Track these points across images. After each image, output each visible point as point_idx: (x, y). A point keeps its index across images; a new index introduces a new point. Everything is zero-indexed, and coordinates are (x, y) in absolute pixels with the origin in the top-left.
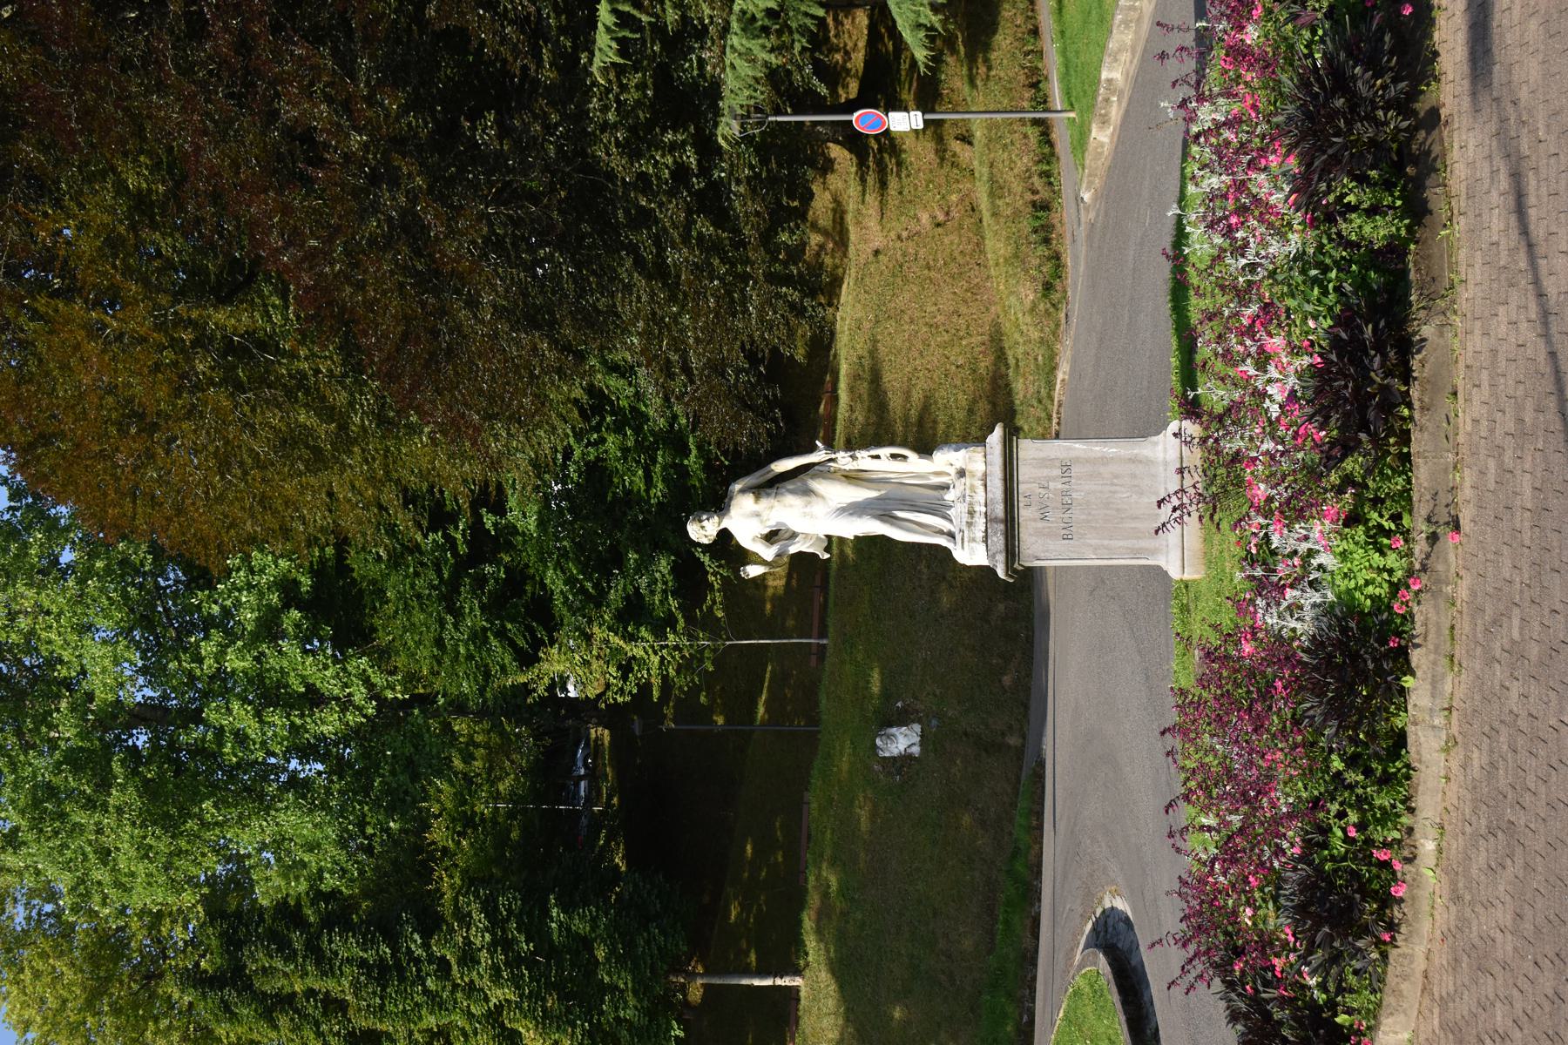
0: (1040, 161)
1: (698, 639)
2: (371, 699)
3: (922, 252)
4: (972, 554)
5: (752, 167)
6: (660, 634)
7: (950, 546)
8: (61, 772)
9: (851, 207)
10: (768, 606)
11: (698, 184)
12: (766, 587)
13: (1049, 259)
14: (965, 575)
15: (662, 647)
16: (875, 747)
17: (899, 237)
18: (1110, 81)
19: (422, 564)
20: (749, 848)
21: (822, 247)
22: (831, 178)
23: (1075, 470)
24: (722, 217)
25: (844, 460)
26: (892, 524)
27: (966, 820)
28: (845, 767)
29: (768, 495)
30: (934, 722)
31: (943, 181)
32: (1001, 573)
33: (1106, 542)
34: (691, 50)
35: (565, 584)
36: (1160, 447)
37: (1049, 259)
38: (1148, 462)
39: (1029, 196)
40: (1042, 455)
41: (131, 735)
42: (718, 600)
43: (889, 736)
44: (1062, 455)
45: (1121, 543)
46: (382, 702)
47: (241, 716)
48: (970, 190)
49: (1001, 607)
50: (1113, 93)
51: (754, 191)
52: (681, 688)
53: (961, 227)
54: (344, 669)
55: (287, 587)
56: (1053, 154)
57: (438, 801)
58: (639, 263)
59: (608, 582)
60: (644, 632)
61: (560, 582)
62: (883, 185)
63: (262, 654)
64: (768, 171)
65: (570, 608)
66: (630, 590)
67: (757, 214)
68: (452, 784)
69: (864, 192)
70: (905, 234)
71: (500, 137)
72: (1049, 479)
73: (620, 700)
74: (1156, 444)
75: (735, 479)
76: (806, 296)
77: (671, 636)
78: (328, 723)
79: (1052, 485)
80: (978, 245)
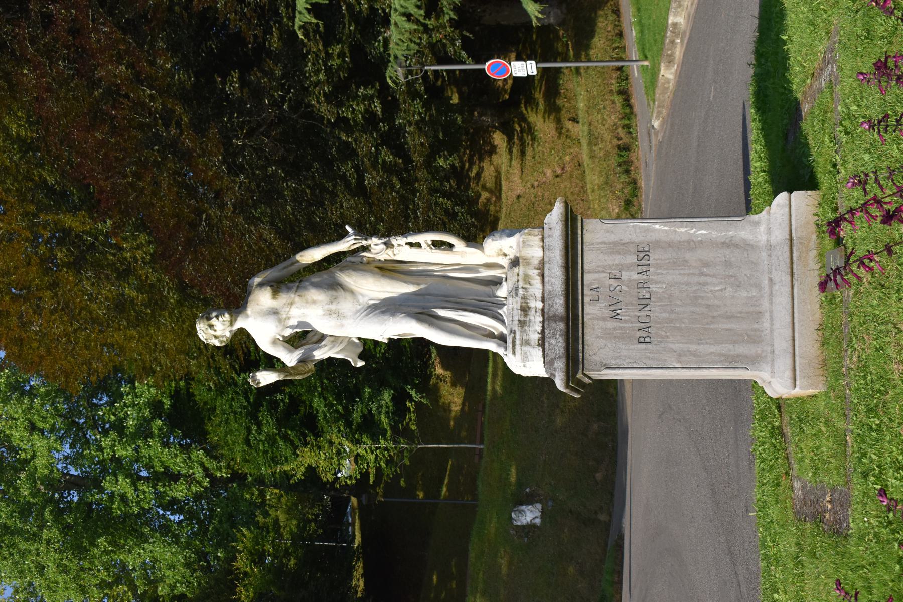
0: (623, 118)
1: (399, 443)
2: (206, 476)
4: (528, 364)
5: (420, 114)
6: (375, 441)
7: (500, 351)
8: (12, 517)
9: (504, 168)
10: (452, 423)
11: (383, 127)
12: (450, 411)
13: (629, 183)
14: (572, 404)
15: (377, 449)
16: (511, 518)
17: (533, 186)
18: (675, 25)
19: (237, 393)
20: (435, 577)
21: (488, 200)
22: (494, 157)
23: (654, 256)
24: (400, 150)
25: (377, 248)
26: (431, 324)
27: (571, 570)
28: (493, 531)
29: (289, 289)
30: (550, 503)
31: (560, 147)
32: (560, 384)
33: (693, 347)
34: (379, 33)
35: (325, 407)
36: (762, 228)
37: (629, 183)
38: (747, 247)
39: (615, 142)
40: (613, 238)
41: (69, 494)
42: (413, 418)
43: (520, 512)
44: (638, 238)
45: (712, 349)
46: (213, 480)
47: (123, 485)
50: (677, 36)
51: (420, 129)
52: (388, 475)
53: (571, 176)
54: (189, 458)
55: (156, 406)
56: (632, 113)
57: (243, 542)
58: (347, 185)
59: (353, 406)
60: (365, 439)
62: (523, 153)
63: (139, 446)
64: (431, 116)
65: (327, 422)
66: (366, 412)
67: (422, 145)
68: (251, 532)
69: (511, 159)
70: (536, 183)
71: (241, 87)
72: (622, 268)
73: (349, 482)
74: (757, 223)
75: (253, 274)
77: (382, 442)
78: (179, 491)
79: (625, 276)
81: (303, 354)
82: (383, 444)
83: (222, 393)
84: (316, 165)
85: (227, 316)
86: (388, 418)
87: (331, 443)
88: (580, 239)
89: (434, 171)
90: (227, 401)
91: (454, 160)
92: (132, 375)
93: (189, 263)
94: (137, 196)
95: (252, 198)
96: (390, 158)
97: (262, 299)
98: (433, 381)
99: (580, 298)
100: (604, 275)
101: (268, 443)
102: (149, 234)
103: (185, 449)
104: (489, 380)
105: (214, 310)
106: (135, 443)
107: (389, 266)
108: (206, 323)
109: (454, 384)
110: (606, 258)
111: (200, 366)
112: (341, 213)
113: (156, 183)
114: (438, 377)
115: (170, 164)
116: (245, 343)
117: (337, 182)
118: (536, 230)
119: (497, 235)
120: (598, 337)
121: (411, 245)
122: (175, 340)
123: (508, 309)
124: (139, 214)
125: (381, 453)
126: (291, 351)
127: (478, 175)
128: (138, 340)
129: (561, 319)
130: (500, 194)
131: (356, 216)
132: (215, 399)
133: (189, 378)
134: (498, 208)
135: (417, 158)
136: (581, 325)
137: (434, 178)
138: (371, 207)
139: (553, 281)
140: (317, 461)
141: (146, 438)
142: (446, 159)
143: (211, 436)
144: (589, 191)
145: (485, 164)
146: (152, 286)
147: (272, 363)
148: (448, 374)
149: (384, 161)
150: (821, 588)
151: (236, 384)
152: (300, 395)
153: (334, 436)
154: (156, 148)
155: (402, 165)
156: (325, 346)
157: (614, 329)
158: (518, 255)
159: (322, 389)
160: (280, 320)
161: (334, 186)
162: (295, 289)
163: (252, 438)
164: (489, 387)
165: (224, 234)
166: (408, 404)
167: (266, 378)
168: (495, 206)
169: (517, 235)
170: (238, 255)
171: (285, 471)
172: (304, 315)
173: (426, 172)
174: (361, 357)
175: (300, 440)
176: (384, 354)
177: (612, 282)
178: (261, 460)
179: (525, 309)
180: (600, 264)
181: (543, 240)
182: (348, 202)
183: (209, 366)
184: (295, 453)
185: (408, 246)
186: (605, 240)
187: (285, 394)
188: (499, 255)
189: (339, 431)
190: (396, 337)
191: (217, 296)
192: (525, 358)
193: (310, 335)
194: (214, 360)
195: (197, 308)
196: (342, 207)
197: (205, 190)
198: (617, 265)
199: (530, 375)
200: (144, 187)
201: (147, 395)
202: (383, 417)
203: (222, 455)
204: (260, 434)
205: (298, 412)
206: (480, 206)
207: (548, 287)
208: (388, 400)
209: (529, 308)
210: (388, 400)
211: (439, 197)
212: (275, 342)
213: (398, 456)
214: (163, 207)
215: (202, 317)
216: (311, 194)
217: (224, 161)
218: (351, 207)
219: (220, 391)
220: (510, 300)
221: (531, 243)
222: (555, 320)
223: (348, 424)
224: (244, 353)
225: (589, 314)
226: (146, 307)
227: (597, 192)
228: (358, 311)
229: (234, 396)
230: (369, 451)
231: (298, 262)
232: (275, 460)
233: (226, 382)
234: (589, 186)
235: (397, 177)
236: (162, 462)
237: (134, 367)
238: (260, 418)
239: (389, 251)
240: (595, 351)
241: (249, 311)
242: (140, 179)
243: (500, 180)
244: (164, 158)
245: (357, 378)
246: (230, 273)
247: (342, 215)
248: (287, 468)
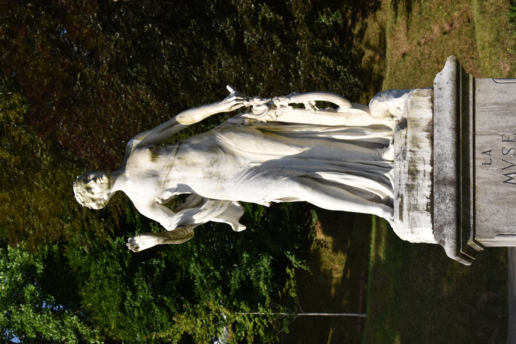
1: (279, 311)
3: (433, 52)
4: (416, 230)
6: (254, 308)
7: (387, 216)
9: (388, 25)
10: (333, 291)
12: (332, 278)
15: (255, 316)
17: (419, 44)
19: (111, 257)
21: (372, 58)
22: (379, 13)
25: (259, 110)
26: (315, 188)
29: (168, 151)
32: (449, 251)
35: (202, 273)
40: (506, 98)
42: (293, 285)
48: (468, 8)
49: (485, 296)
53: (460, 33)
54: (63, 324)
55: (28, 271)
58: (226, 43)
59: (231, 272)
60: (243, 306)
61: (199, 271)
62: (409, 9)
63: (11, 312)
65: (204, 288)
66: (244, 278)
69: (396, 16)
70: (423, 41)
75: (134, 135)
76: (340, 64)
77: (261, 309)
80: (472, 45)
81: (183, 218)
82: (261, 311)
83: (96, 258)
84: (193, 22)
85: (105, 179)
86: (267, 284)
87: (208, 310)
88: (471, 100)
89: (317, 30)
90: (102, 265)
91: (336, 17)
92: (4, 238)
93: (64, 123)
94: (10, 55)
95: (128, 57)
96: (270, 15)
97: (141, 161)
98: (313, 247)
99: (471, 161)
100: (497, 137)
101: (143, 309)
102: (22, 94)
103: (59, 315)
104: (372, 246)
105: (92, 173)
106: (6, 309)
107: (272, 127)
108: (84, 185)
109: (335, 250)
110: (499, 119)
111: (74, 230)
112: (219, 72)
113: (30, 41)
114: (319, 242)
115: (44, 22)
116: (120, 206)
117: (215, 40)
118: (425, 90)
119: (384, 96)
120: (490, 202)
121: (293, 105)
122: (48, 203)
123: (395, 172)
124: (12, 73)
125: (259, 320)
126: (170, 215)
127: (362, 33)
128: (11, 203)
129: (451, 183)
130: (385, 52)
131: (235, 75)
132: (90, 264)
133: (62, 241)
134: (382, 67)
135: (299, 15)
136: (472, 190)
137: (316, 36)
138: (250, 66)
139: (442, 143)
140: (193, 329)
141: (18, 304)
142: (329, 15)
143: (85, 301)
144: (479, 48)
145: (369, 20)
146: (25, 147)
147: (148, 226)
148: (329, 239)
149: (264, 18)
150: (456, 47)
151: (110, 248)
152: (177, 260)
153: (211, 303)
154: (29, 4)
155: (283, 23)
156: (205, 210)
157: (508, 194)
158: (406, 116)
159: (199, 254)
160: (159, 183)
161: (213, 44)
162: (174, 151)
163: (126, 304)
164: (372, 254)
165: (99, 94)
166: (288, 270)
167: (145, 242)
168: (379, 64)
169: (405, 96)
170: (113, 115)
171: (161, 338)
172: (184, 178)
173: (307, 30)
174: (242, 221)
175: (176, 307)
176: (263, 218)
177: (505, 144)
178: (136, 328)
179: (413, 173)
180: (493, 126)
181: (432, 101)
182: (226, 62)
183: (83, 230)
184: (171, 320)
185: (291, 107)
186: (499, 101)
187: (161, 259)
188: (385, 116)
189: (217, 297)
190: (278, 201)
191: (91, 158)
192: (413, 224)
193: (189, 198)
194: (89, 224)
195: (71, 170)
196: (220, 66)
197: (78, 48)
198: (511, 127)
199: (418, 241)
200: (17, 46)
201: (19, 259)
202: (261, 283)
203: (96, 321)
204: (135, 300)
205: (174, 277)
206: (363, 64)
207: (437, 150)
208: (266, 266)
209: (418, 172)
210: (266, 266)
211: (321, 56)
212: (154, 205)
213: (277, 324)
214: (37, 65)
215: (80, 179)
216: (189, 53)
217: (99, 19)
218: (230, 66)
219: (95, 255)
220: (397, 163)
221: (420, 104)
222: (445, 185)
223: (226, 291)
224: (122, 216)
225: (480, 178)
226: (20, 169)
227: (488, 50)
228: (239, 174)
229: (109, 260)
230: (247, 319)
231: (178, 123)
232: (150, 328)
233: (100, 245)
234: (478, 43)
235: (278, 34)
236: (35, 328)
237: (6, 231)
238: (136, 284)
239: (272, 113)
240: (487, 217)
241: (128, 173)
242: (12, 36)
243: (385, 38)
244: (38, 15)
245: (235, 244)
246: (105, 134)
247: (221, 75)
248: (162, 335)
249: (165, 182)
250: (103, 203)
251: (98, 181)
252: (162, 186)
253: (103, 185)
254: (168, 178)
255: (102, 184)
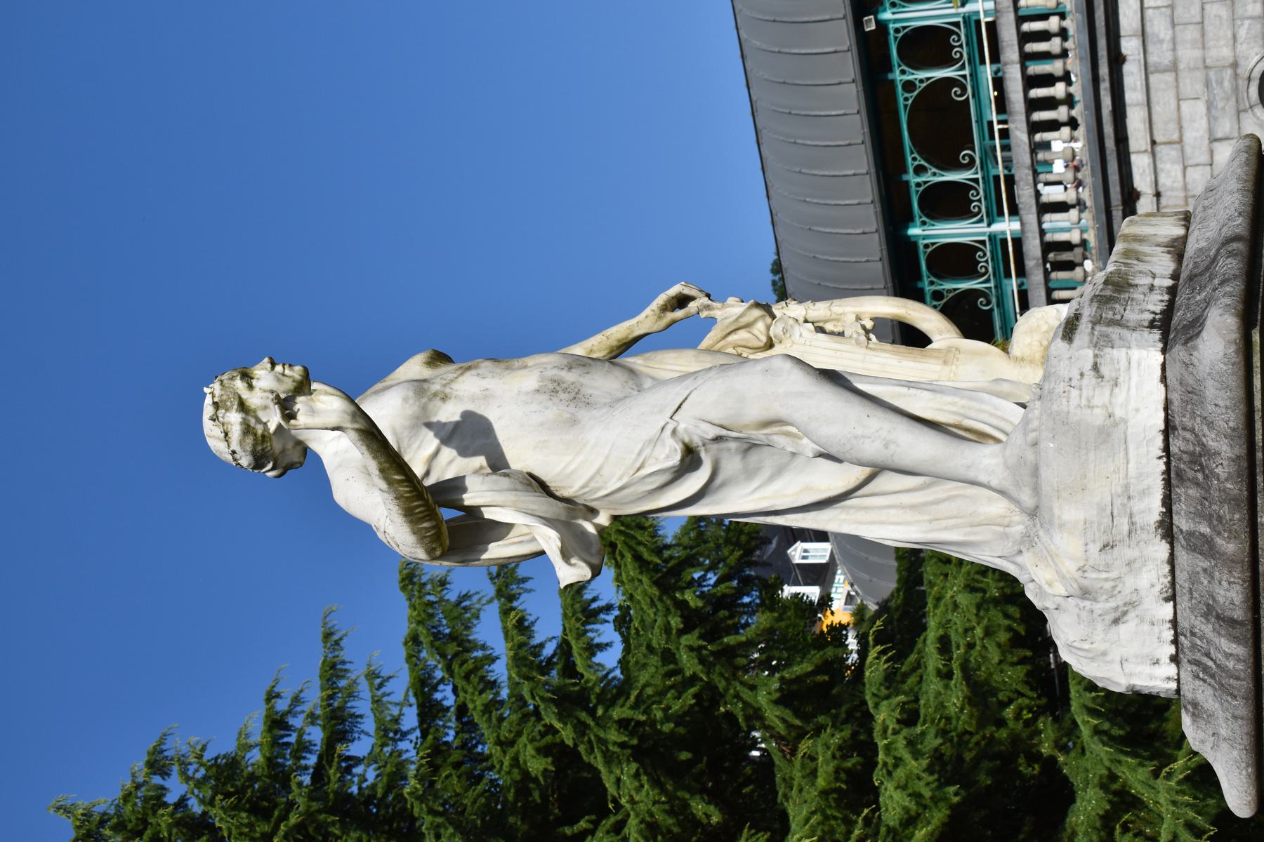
181: (1177, 80)
249: (435, 395)
250: (260, 432)
251: (279, 368)
252: (424, 400)
253: (286, 379)
254: (447, 390)
255: (283, 375)
